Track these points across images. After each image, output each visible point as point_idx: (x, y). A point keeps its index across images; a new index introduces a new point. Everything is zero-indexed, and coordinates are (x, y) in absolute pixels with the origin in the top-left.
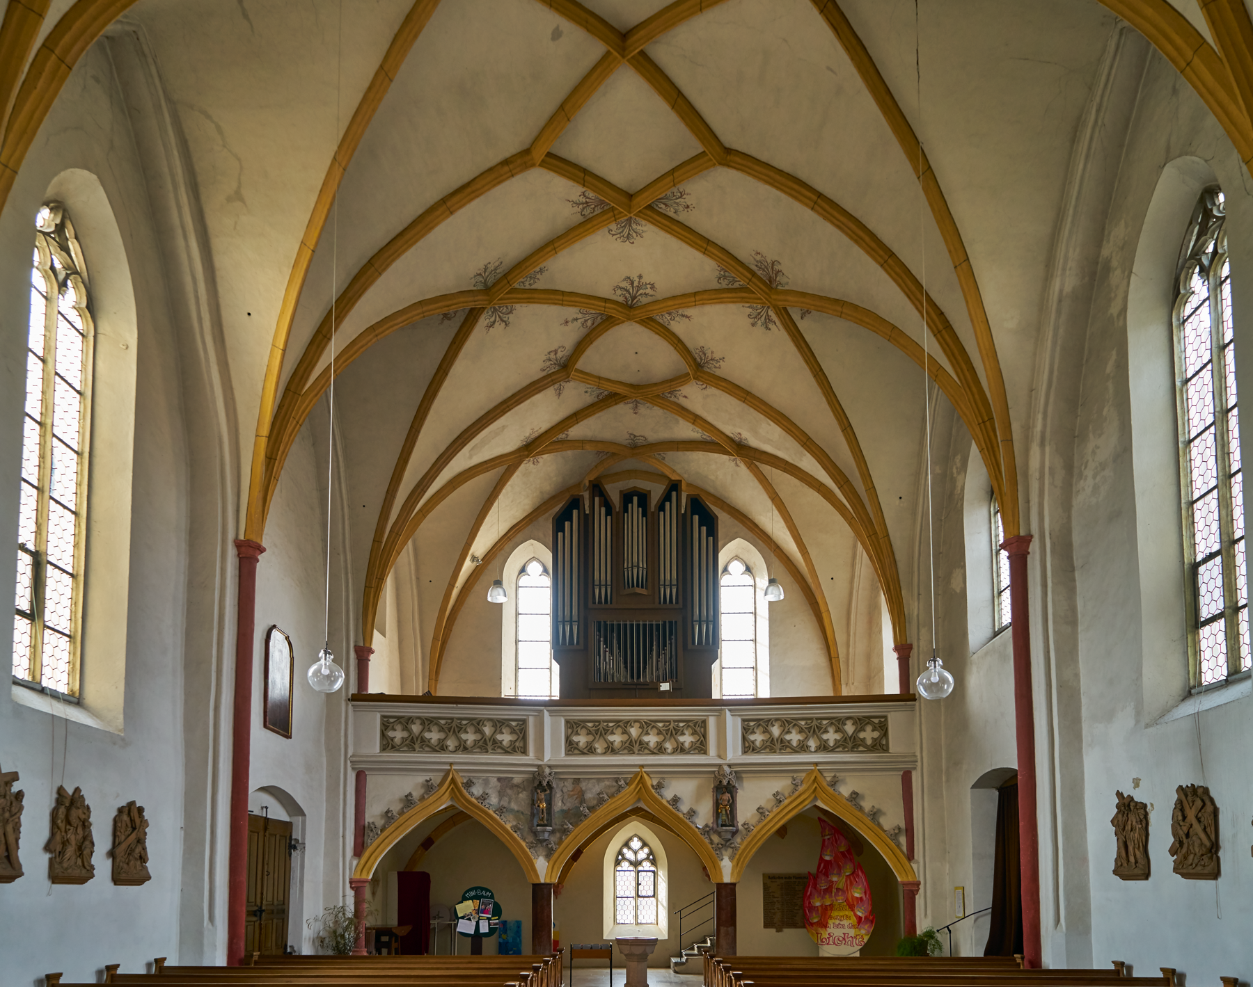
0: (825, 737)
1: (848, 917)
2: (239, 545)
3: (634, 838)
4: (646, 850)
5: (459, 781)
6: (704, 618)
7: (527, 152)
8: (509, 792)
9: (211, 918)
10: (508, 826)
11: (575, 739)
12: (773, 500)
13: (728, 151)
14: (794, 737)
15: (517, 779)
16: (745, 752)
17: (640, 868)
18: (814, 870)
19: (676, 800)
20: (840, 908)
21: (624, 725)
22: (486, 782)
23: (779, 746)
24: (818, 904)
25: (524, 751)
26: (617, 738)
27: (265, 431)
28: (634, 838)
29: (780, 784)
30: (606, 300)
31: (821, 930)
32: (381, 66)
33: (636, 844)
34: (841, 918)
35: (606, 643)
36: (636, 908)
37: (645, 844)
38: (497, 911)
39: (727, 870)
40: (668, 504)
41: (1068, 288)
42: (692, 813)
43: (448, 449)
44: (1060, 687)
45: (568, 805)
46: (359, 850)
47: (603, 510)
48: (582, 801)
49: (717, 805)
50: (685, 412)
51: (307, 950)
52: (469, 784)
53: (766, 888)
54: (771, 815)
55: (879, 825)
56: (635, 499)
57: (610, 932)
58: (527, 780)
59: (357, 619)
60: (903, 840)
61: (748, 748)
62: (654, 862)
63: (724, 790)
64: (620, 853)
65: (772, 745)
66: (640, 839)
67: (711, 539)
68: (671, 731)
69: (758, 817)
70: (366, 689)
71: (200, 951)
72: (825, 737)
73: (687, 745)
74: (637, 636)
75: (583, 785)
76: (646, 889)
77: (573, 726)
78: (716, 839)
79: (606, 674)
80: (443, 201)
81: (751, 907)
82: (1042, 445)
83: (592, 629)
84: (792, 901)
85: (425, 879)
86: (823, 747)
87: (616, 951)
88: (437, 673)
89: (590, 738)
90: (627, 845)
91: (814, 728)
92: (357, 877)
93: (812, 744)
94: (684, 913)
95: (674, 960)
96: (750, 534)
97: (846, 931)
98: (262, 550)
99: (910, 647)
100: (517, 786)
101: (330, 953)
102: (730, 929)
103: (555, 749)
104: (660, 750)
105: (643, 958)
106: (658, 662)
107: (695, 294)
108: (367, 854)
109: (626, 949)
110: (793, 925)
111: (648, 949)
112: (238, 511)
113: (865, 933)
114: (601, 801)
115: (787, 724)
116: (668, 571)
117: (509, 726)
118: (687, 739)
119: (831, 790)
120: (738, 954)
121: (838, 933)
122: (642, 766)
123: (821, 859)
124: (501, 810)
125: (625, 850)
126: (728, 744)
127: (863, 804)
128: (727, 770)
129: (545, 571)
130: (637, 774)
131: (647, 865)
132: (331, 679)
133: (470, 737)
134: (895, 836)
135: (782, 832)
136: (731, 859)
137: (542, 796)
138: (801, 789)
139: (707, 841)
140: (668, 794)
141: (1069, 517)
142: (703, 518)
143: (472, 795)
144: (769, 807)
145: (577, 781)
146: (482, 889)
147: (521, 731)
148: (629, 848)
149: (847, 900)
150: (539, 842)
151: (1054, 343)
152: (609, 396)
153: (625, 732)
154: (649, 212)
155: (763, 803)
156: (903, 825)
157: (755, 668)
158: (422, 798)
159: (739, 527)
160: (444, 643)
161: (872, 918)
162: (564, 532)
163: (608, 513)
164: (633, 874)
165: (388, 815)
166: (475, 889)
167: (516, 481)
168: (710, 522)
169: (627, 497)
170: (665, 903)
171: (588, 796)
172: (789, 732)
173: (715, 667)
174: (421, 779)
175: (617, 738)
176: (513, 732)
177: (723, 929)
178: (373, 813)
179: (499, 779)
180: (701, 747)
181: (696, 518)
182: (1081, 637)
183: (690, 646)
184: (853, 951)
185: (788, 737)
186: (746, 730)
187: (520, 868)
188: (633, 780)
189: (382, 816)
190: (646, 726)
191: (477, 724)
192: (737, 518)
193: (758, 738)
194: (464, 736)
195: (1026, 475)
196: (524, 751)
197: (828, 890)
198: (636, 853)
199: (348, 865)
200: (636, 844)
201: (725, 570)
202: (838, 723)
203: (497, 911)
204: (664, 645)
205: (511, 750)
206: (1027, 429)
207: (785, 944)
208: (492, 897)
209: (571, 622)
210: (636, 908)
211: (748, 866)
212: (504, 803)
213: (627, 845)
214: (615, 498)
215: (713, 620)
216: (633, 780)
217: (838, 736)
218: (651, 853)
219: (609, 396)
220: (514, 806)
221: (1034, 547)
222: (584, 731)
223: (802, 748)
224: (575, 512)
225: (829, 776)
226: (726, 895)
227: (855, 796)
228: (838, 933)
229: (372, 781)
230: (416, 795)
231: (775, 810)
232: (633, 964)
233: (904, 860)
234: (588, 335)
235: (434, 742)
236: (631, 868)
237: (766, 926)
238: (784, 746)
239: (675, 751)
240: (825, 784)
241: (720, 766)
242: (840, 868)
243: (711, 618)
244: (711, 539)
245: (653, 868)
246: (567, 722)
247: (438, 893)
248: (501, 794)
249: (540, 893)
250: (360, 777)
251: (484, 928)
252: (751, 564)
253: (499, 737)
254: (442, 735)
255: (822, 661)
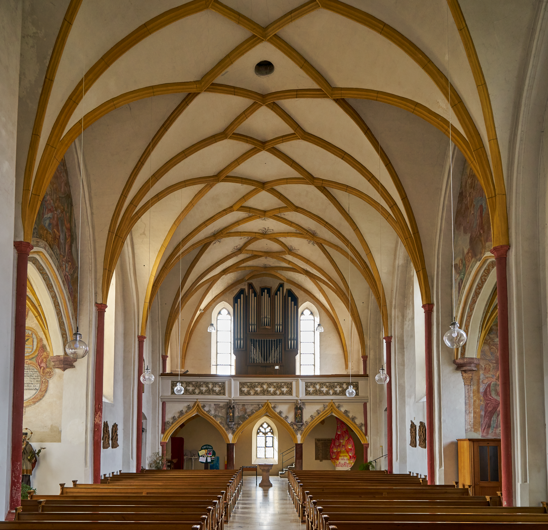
0: (336, 389)
1: (346, 456)
2: (139, 337)
3: (264, 423)
4: (269, 428)
5: (200, 405)
6: (293, 338)
7: (231, 207)
8: (219, 409)
9: (132, 458)
10: (218, 422)
11: (243, 389)
12: (320, 291)
13: (297, 207)
14: (325, 389)
15: (221, 404)
16: (306, 395)
17: (267, 435)
18: (334, 437)
19: (280, 413)
20: (343, 453)
21: (261, 384)
22: (210, 405)
23: (319, 392)
24: (335, 451)
25: (224, 394)
26: (259, 389)
27: (148, 301)
28: (264, 423)
29: (319, 407)
30: (256, 233)
31: (336, 461)
32: (191, 202)
33: (265, 425)
34: (344, 456)
35: (254, 346)
36: (265, 451)
37: (269, 426)
38: (214, 454)
39: (299, 439)
40: (278, 292)
41: (400, 264)
42: (286, 417)
43: (196, 280)
44: (399, 385)
45: (240, 414)
46: (163, 431)
47: (253, 294)
48: (246, 413)
49: (296, 414)
50: (285, 260)
51: (147, 468)
52: (204, 406)
53: (316, 444)
54: (316, 418)
55: (355, 423)
56: (266, 291)
57: (255, 461)
58: (225, 405)
59: (162, 345)
60: (363, 428)
61: (308, 393)
62: (272, 433)
63: (298, 409)
64: (259, 429)
65: (316, 392)
66: (267, 423)
67: (295, 307)
68: (279, 386)
69: (311, 419)
70: (165, 371)
71: (129, 468)
72: (336, 389)
73: (285, 392)
74: (267, 347)
75: (246, 407)
76: (269, 444)
77: (242, 385)
78: (295, 427)
79: (254, 359)
80: (204, 223)
81: (309, 452)
82: (395, 308)
83: (249, 342)
84: (326, 450)
85: (181, 440)
86: (335, 393)
87: (258, 468)
88: (185, 356)
89: (249, 389)
90: (261, 426)
91: (332, 386)
92: (163, 441)
93: (331, 392)
94: (284, 454)
95: (280, 472)
96: (312, 300)
97: (346, 461)
98: (145, 338)
99: (367, 357)
100: (221, 407)
101: (154, 469)
102: (300, 461)
103: (235, 393)
104: (275, 394)
105: (268, 471)
106: (274, 355)
107: (288, 233)
108: (166, 433)
109: (262, 468)
110: (327, 459)
111: (270, 468)
112: (138, 326)
113: (352, 462)
114: (253, 413)
115: (322, 384)
116: (279, 320)
117: (218, 384)
118: (285, 389)
119: (337, 409)
120: (304, 469)
121: (342, 462)
122: (268, 400)
123: (337, 434)
124: (215, 416)
125: (261, 428)
126: (300, 392)
127: (349, 414)
128: (299, 401)
129: (229, 313)
130: (266, 403)
131: (270, 434)
132: (181, 390)
133: (204, 389)
134: (360, 427)
135: (323, 422)
136: (301, 434)
137: (231, 411)
138: (326, 409)
139: (292, 428)
140: (278, 410)
141: (403, 332)
142: (292, 299)
143: (205, 410)
144: (315, 415)
145: (244, 405)
146: (209, 445)
147: (223, 386)
148: (263, 427)
149: (346, 449)
150: (229, 428)
151: (397, 279)
152: (255, 256)
153: (262, 387)
154: (272, 150)
155: (313, 414)
156: (363, 423)
157: (314, 354)
158: (186, 412)
159: (308, 297)
160: (188, 343)
161: (355, 457)
162: (237, 303)
163: (255, 296)
164: (264, 438)
165: (174, 418)
166: (206, 445)
167: (219, 282)
168: (295, 300)
169: (262, 290)
170: (277, 450)
171: (248, 411)
172: (322, 387)
173: (297, 357)
174: (186, 404)
175: (259, 389)
176: (220, 387)
177: (298, 461)
178: (168, 418)
179: (215, 405)
180: (290, 393)
181: (290, 298)
182: (406, 370)
183: (287, 349)
184: (348, 468)
185: (322, 389)
186: (307, 386)
187: (222, 437)
188: (264, 405)
189: (172, 419)
190: (270, 384)
191: (207, 384)
192: (307, 293)
193: (311, 389)
194: (201, 388)
195: (391, 317)
196: (224, 394)
197: (339, 446)
198: (265, 429)
199: (160, 437)
200: (265, 425)
201: (302, 313)
202: (341, 384)
203: (214, 454)
204: (277, 347)
205: (219, 393)
206: (391, 305)
207: (324, 466)
208: (212, 448)
209: (240, 339)
210: (265, 451)
211: (308, 435)
212: (217, 413)
213: (261, 426)
214: (258, 290)
215: (296, 339)
216: (264, 405)
217: (340, 389)
218: (271, 429)
219: (255, 256)
220: (220, 414)
221: (393, 340)
222: (246, 386)
223: (327, 393)
224: (242, 295)
225: (337, 404)
226: (299, 448)
227: (346, 412)
228: (342, 462)
229: (168, 405)
230: (184, 410)
231: (317, 417)
232: (265, 473)
233: (363, 436)
234: (249, 241)
235: (191, 390)
236: (263, 435)
237: (316, 459)
238: (320, 392)
239: (280, 394)
240: (335, 407)
241: (297, 400)
242: (343, 437)
243: (295, 338)
244: (295, 307)
245: (272, 435)
246: (240, 383)
247: (188, 446)
248: (215, 410)
249: (230, 447)
250: (164, 404)
251: (209, 460)
252: (313, 311)
253: (215, 389)
254: (193, 388)
255: (341, 352)
